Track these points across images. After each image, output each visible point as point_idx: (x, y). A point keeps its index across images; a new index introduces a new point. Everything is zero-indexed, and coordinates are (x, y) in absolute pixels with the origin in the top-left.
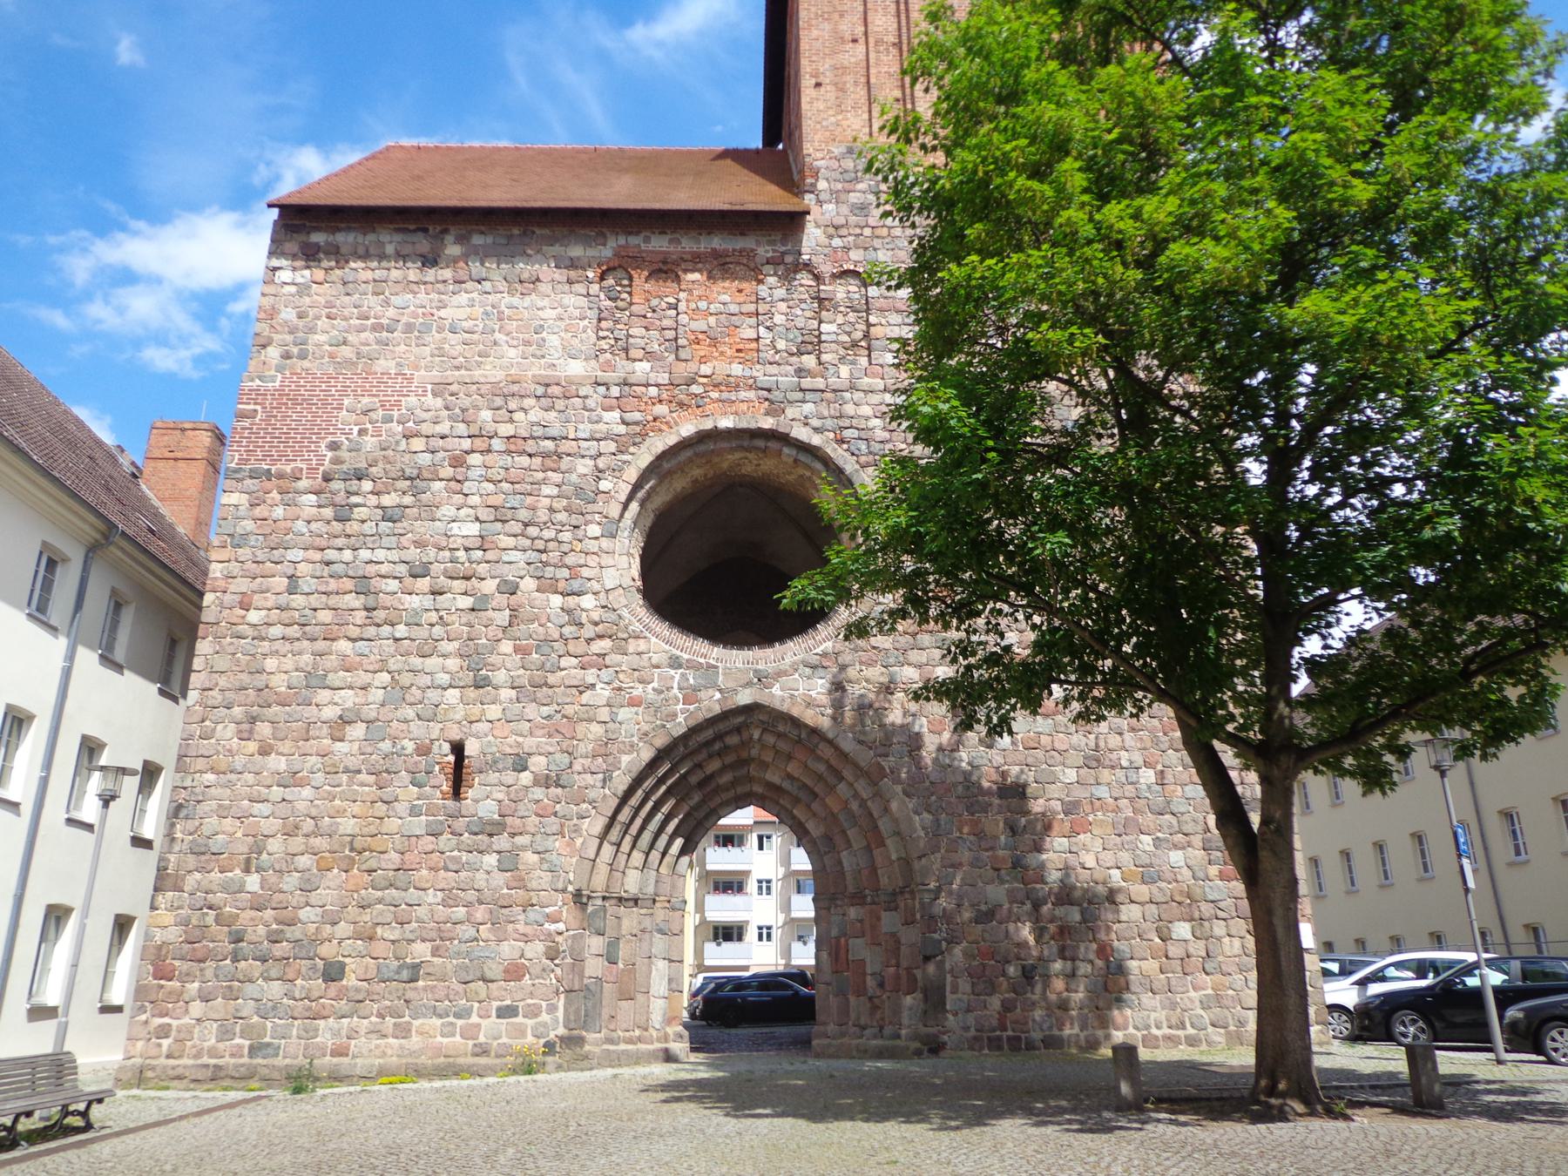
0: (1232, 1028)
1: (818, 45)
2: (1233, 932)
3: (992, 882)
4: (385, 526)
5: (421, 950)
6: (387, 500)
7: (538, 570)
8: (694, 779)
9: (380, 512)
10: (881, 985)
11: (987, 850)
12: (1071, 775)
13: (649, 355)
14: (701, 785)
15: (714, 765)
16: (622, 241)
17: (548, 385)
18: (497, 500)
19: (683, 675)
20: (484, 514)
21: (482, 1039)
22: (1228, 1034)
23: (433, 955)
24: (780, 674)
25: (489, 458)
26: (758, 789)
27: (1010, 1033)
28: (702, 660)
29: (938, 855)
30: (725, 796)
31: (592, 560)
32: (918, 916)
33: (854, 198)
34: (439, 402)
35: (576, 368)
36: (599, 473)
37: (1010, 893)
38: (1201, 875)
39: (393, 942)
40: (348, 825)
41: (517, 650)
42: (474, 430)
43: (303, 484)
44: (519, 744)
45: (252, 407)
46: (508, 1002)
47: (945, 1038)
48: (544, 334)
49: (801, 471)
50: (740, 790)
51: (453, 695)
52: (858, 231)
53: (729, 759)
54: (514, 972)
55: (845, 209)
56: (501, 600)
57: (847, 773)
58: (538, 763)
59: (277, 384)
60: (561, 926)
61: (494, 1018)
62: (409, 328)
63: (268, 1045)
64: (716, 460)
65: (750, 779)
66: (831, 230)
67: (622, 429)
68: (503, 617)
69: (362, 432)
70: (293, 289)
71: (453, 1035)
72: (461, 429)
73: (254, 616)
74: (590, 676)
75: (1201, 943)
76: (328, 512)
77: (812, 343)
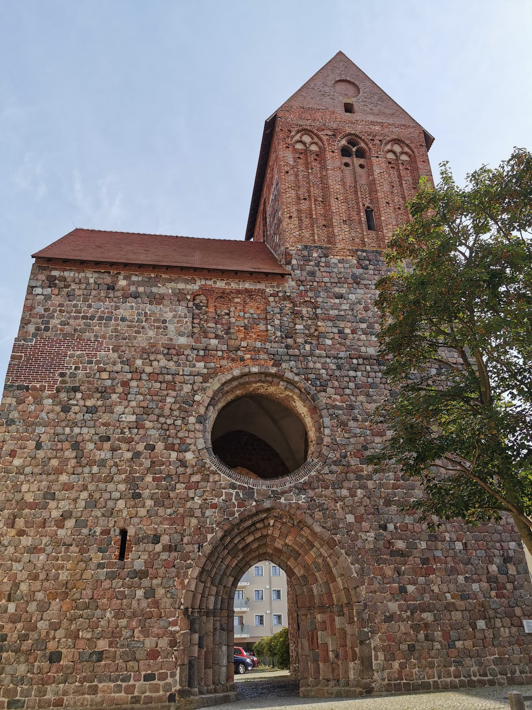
0: (509, 675)
1: (289, 200)
2: (505, 625)
3: (391, 600)
4: (88, 416)
5: (102, 645)
6: (89, 403)
7: (165, 438)
8: (240, 546)
9: (85, 409)
10: (337, 656)
11: (387, 584)
12: (423, 545)
13: (217, 337)
14: (243, 549)
15: (250, 539)
16: (203, 282)
17: (169, 349)
18: (144, 404)
19: (237, 493)
20: (138, 410)
21: (136, 694)
22: (507, 678)
23: (109, 647)
24: (283, 493)
25: (140, 383)
26: (270, 551)
27: (405, 681)
28: (246, 485)
29: (364, 587)
30: (253, 555)
31: (192, 435)
32: (356, 619)
33: (308, 268)
34: (116, 355)
35: (183, 340)
36: (195, 392)
37: (400, 606)
38: (488, 595)
39: (88, 639)
40: (64, 576)
41: (154, 479)
42: (133, 369)
43: (47, 393)
44: (156, 529)
45: (20, 354)
46: (150, 672)
47: (373, 685)
48: (167, 324)
49: (287, 393)
50: (261, 551)
51: (121, 504)
52: (311, 283)
53: (258, 535)
54: (153, 654)
55: (304, 273)
56: (147, 453)
57: (316, 544)
58: (165, 539)
59: (33, 343)
60: (177, 628)
61: (142, 682)
62: (101, 318)
63: (18, 701)
64: (248, 386)
65: (265, 545)
66: (299, 283)
67: (205, 371)
68: (147, 463)
69: (77, 368)
70: (43, 297)
71: (120, 692)
72: (127, 368)
73: (17, 462)
74: (191, 493)
75: (491, 631)
76: (58, 408)
77: (290, 334)
